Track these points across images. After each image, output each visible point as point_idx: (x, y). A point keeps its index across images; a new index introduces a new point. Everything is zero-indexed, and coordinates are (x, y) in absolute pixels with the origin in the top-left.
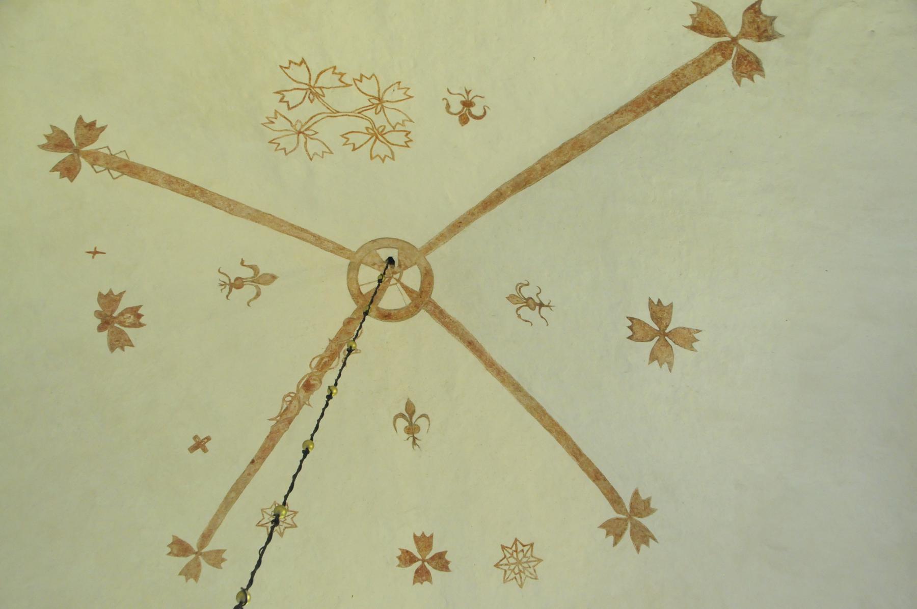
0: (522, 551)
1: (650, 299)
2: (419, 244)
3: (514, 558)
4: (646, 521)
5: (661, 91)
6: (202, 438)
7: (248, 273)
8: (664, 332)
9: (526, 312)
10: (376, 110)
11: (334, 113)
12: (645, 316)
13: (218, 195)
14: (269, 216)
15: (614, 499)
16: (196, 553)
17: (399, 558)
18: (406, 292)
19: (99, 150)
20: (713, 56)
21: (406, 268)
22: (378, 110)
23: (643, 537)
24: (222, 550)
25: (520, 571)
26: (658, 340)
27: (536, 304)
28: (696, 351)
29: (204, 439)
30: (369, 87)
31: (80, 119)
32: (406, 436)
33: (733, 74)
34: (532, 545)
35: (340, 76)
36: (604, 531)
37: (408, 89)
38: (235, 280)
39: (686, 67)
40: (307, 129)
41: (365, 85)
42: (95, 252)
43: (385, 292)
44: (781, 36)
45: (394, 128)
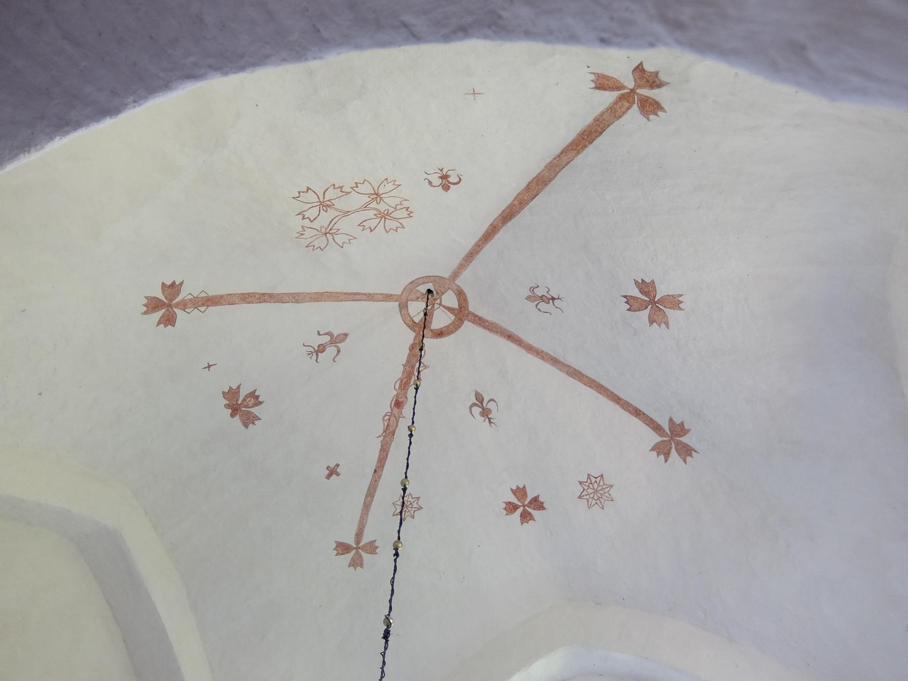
0: (596, 482)
1: (634, 280)
2: (447, 276)
3: (591, 489)
4: (685, 439)
5: (591, 133)
7: (326, 339)
8: (654, 301)
9: (542, 306)
10: (377, 201)
11: (347, 213)
12: (636, 293)
13: (283, 294)
14: (327, 294)
15: (656, 428)
16: (356, 548)
17: (505, 509)
18: (449, 311)
19: (185, 298)
20: (620, 103)
21: (443, 293)
22: (379, 201)
23: (686, 452)
24: (374, 541)
26: (651, 307)
27: (549, 299)
28: (684, 310)
29: (335, 466)
30: (365, 188)
31: (163, 284)
32: (483, 419)
33: (641, 113)
34: (602, 476)
35: (340, 189)
36: (655, 453)
37: (395, 181)
38: (318, 348)
39: (602, 114)
41: (361, 188)
42: (209, 366)
43: (433, 316)
44: (667, 83)
45: (395, 208)
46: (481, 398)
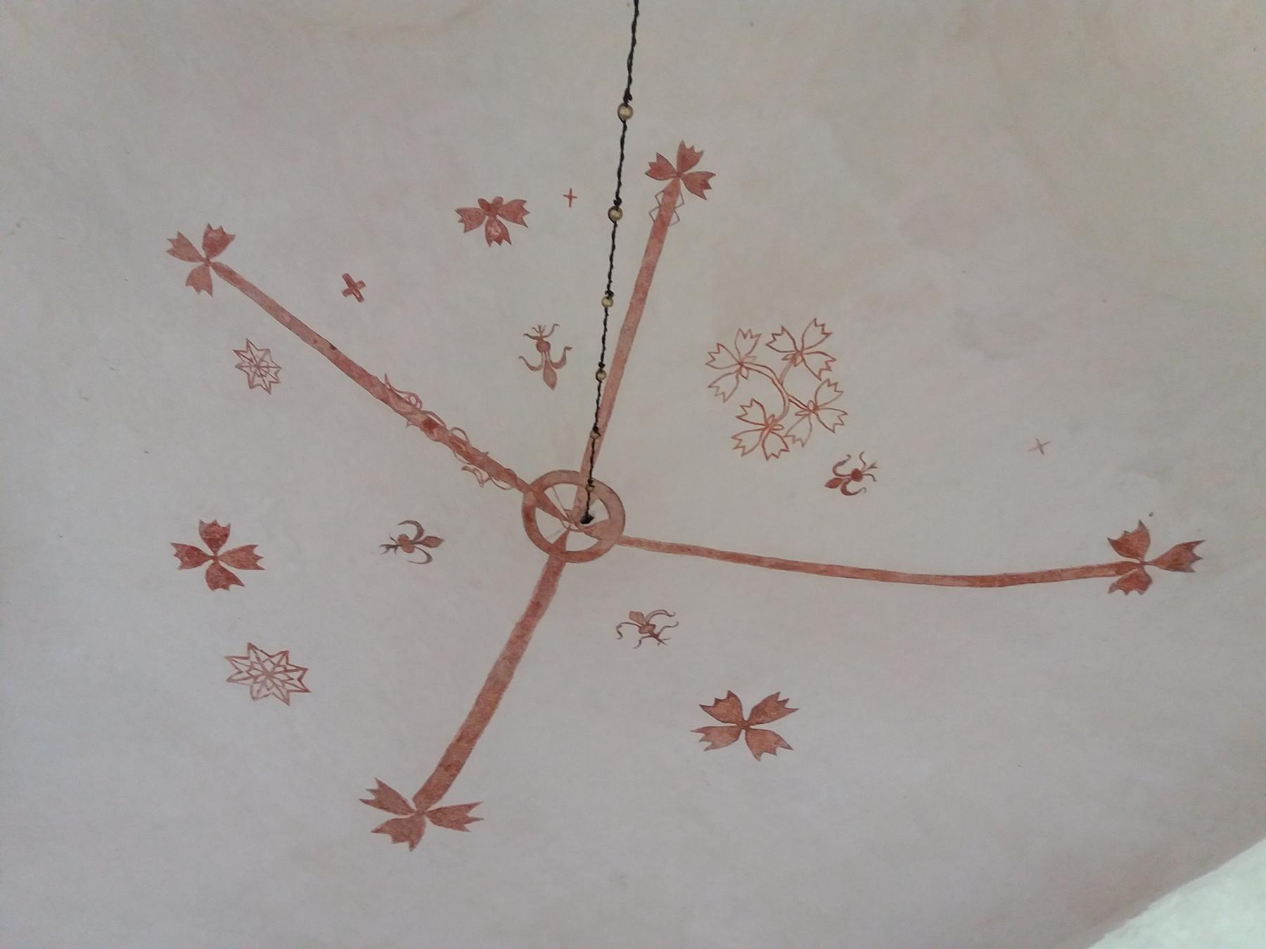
6: (361, 291)
7: (555, 356)
10: (802, 411)
16: (208, 260)
19: (680, 197)
25: (256, 678)
29: (360, 295)
30: (826, 395)
32: (396, 538)
40: (748, 369)
42: (570, 197)
46: (431, 545)
